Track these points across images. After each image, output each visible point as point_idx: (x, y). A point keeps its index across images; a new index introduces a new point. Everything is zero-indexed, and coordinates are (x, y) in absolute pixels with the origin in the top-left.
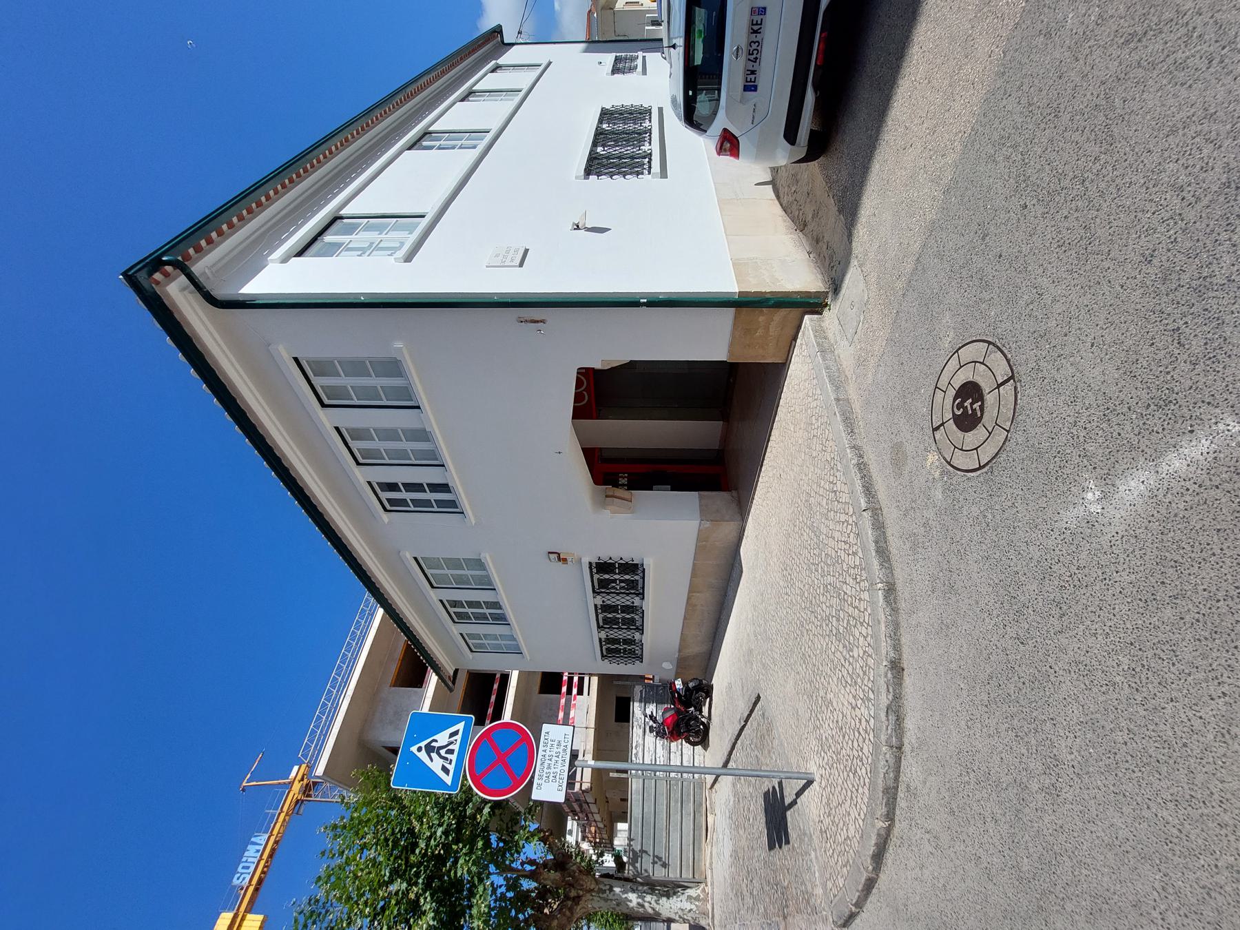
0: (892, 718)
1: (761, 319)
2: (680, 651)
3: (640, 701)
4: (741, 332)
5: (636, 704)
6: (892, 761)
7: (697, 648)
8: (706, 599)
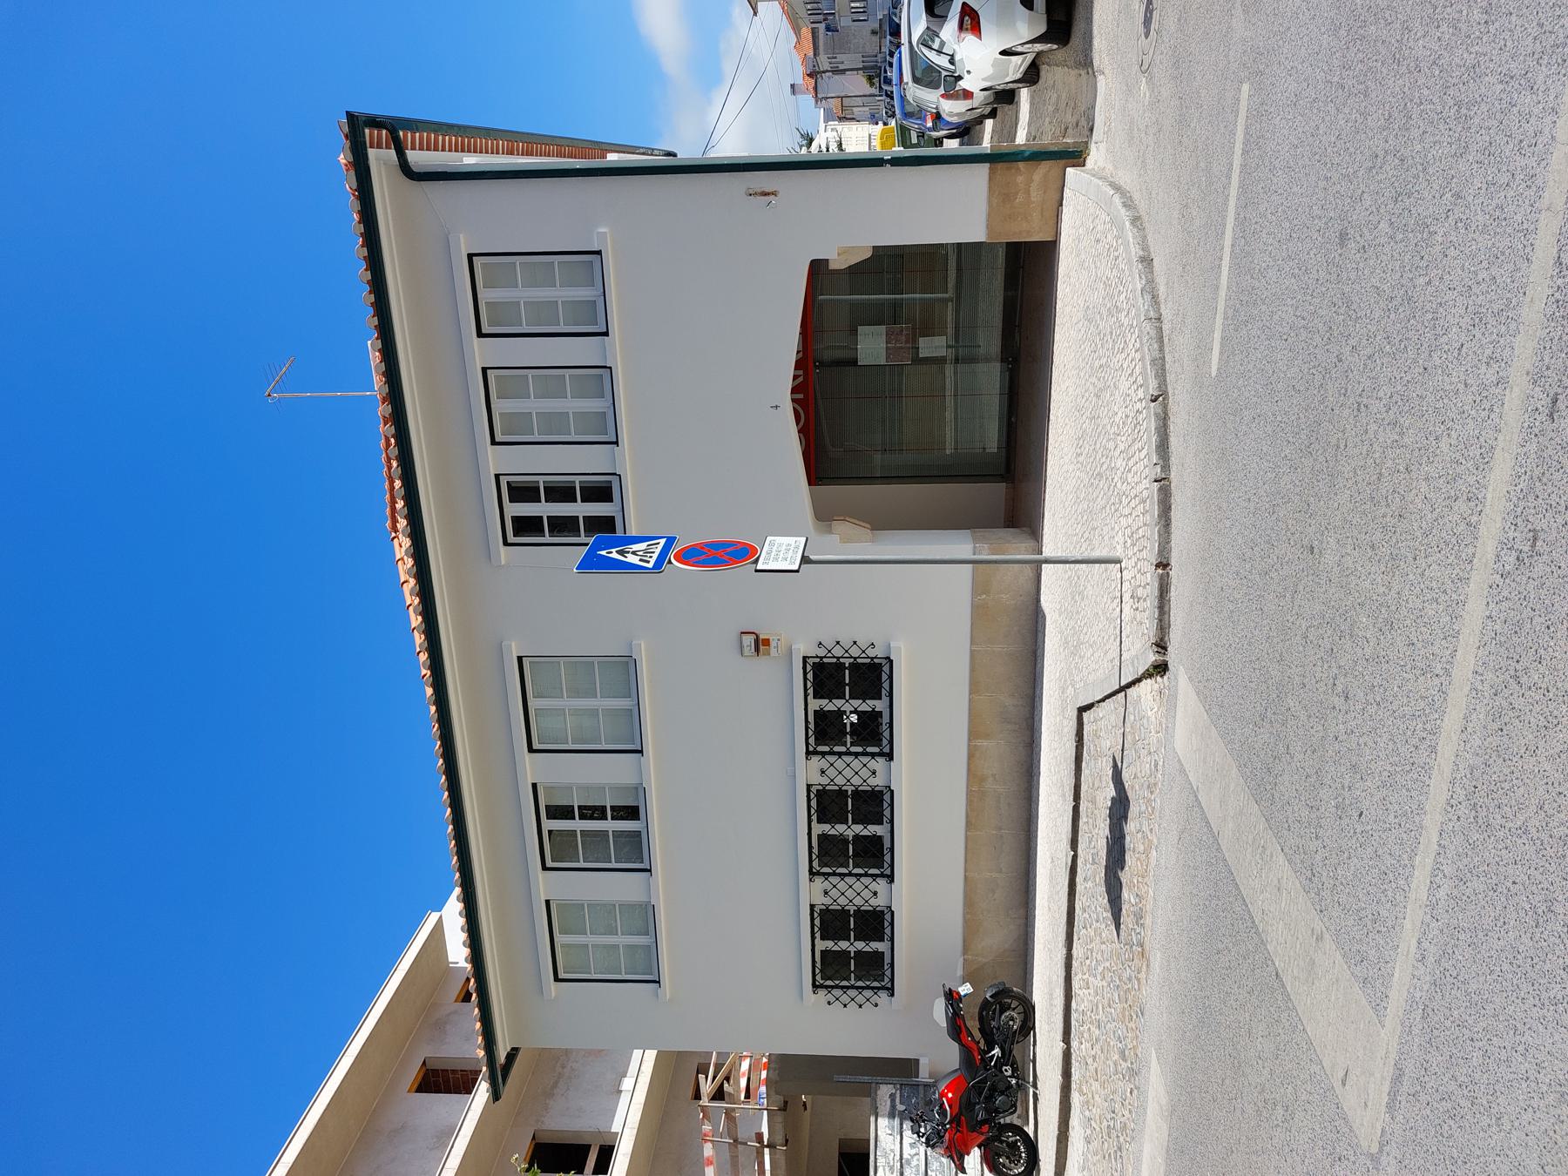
0: (1148, 297)
1: (1020, 179)
2: (966, 948)
3: (892, 1115)
4: (1001, 197)
5: (883, 1122)
6: (1153, 333)
7: (996, 939)
8: (999, 750)
